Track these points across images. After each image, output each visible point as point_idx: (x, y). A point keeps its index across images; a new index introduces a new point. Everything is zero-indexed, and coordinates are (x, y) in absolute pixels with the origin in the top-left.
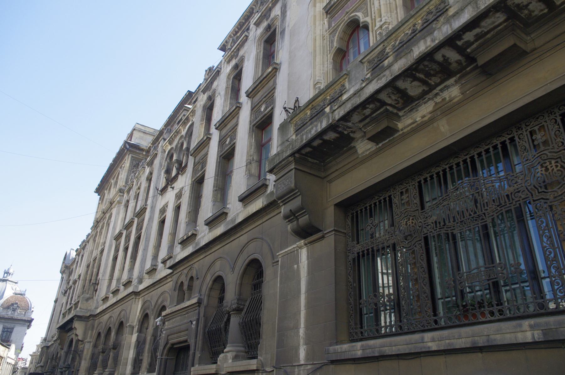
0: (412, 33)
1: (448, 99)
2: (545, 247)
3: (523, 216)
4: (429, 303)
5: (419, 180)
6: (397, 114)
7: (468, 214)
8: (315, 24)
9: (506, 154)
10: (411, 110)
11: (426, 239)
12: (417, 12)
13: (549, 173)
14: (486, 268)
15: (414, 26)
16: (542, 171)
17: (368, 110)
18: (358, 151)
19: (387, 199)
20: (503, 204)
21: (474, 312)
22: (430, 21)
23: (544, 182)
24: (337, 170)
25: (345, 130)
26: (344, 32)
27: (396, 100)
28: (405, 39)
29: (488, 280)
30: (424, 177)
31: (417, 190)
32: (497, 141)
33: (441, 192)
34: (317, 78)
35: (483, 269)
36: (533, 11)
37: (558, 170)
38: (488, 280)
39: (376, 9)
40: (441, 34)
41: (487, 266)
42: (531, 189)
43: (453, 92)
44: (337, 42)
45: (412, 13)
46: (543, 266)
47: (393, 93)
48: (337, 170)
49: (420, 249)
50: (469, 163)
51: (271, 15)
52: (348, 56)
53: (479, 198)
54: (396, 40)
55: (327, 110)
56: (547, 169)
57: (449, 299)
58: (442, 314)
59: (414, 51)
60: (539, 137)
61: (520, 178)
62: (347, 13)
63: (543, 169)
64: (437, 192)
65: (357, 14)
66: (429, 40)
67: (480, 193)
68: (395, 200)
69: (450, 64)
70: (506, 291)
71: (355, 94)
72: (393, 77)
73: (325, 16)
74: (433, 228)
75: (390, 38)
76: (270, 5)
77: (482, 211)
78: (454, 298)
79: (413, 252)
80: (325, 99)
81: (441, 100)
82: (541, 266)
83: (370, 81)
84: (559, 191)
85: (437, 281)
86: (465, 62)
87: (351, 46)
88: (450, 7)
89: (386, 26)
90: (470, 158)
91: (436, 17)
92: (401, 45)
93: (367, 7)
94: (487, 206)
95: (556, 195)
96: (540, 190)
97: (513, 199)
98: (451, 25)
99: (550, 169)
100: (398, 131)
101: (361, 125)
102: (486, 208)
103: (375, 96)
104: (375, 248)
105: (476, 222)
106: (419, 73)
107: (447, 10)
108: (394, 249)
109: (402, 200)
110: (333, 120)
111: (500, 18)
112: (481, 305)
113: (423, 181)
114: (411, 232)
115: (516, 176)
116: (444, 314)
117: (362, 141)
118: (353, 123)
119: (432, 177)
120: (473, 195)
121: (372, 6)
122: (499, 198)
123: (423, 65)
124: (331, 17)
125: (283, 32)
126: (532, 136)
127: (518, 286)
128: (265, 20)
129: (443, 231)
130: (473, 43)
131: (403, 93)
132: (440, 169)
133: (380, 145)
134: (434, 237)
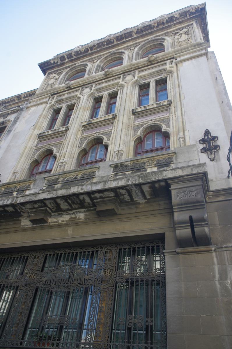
0: (74, 179)
1: (77, 218)
2: (91, 313)
3: (87, 293)
4: (23, 329)
5: (47, 254)
6: (50, 214)
7: (63, 283)
8: (30, 139)
9: (92, 257)
10: (59, 215)
11: (37, 289)
12: (80, 171)
13: (106, 275)
14: (60, 317)
15: (77, 176)
16: (103, 273)
17: (37, 205)
18: (22, 223)
19: (26, 257)
20: (81, 284)
21: (44, 341)
22: (84, 178)
23: (102, 279)
24: (4, 229)
25: (20, 210)
26: (43, 153)
27: (53, 207)
28: (70, 180)
29: (59, 324)
30: (50, 253)
31: (44, 259)
32: (91, 250)
33: (55, 265)
34: (17, 170)
35: (58, 317)
36: (125, 198)
37: (109, 275)
38: (59, 324)
39: (64, 152)
40: (86, 189)
41: (61, 315)
42: (96, 280)
43: (81, 216)
44: (37, 156)
45: (79, 169)
46: (86, 323)
47: (53, 203)
48: (4, 229)
49: (31, 295)
50: (74, 255)
51: (7, 118)
52: (40, 166)
53: (72, 276)
54: (66, 177)
55: (15, 194)
56: (105, 273)
57: (35, 329)
58: (26, 339)
59: (71, 189)
60: (108, 255)
61: (93, 273)
62: (49, 144)
63: (104, 272)
64: (53, 264)
65: (54, 148)
66: (80, 187)
67: (73, 273)
68: (30, 260)
69: (85, 202)
70: (65, 332)
71: (34, 194)
72: (56, 196)
73: (37, 138)
74: (43, 285)
75: (64, 175)
76: (10, 112)
77: (70, 284)
78: (37, 330)
79: (27, 295)
80: (16, 187)
81: (74, 217)
82: (86, 322)
83: (44, 192)
84: (106, 286)
85: (33, 316)
86: (92, 205)
87: (43, 162)
88: (95, 177)
89: (65, 164)
90: (76, 252)
91: (87, 178)
92: (67, 181)
93: (60, 147)
94: (74, 282)
95: (104, 288)
96: (99, 283)
97: (86, 283)
98: (92, 187)
99: (107, 274)
100: (47, 222)
101: (29, 211)
102: (73, 283)
103: (44, 201)
104: (6, 285)
105: (65, 289)
106: (69, 200)
107: (93, 178)
108: (17, 289)
109: (33, 261)
110: (16, 202)
111: (112, 194)
112: (50, 338)
113: (48, 255)
114: (30, 282)
115: (92, 271)
116: (28, 339)
117: (26, 219)
118: (26, 208)
119: (54, 255)
120: (70, 273)
121: (63, 149)
122: (81, 279)
123: (73, 197)
124: (40, 141)
125: (10, 131)
126: (105, 254)
127: (71, 330)
128: (2, 118)
129: (47, 289)
130: (98, 199)
131: (58, 206)
132: (59, 252)
133: (35, 226)
134: (41, 289)
